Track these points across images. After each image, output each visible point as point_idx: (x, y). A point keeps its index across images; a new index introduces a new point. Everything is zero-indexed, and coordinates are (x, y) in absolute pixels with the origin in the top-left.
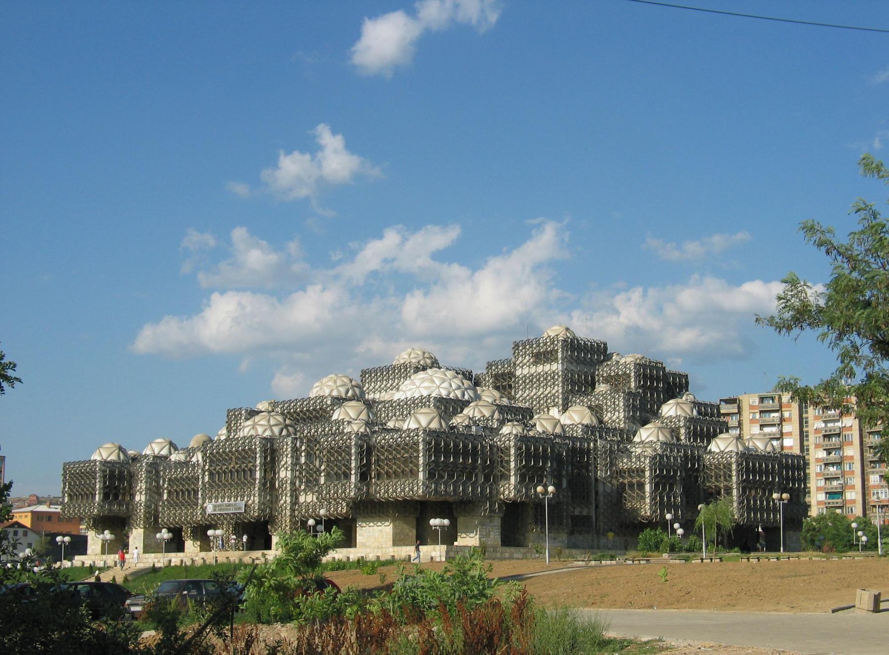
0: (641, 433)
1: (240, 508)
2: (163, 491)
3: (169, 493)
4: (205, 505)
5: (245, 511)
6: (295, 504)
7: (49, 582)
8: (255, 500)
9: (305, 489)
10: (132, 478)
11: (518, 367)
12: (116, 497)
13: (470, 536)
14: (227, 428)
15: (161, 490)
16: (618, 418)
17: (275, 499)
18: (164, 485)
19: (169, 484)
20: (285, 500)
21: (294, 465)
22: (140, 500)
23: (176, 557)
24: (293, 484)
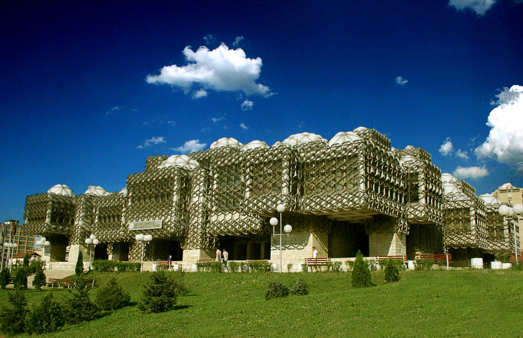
0: (449, 177)
1: (158, 225)
2: (95, 218)
3: (100, 218)
4: (128, 224)
5: (162, 228)
6: (206, 223)
7: (153, 138)
8: (172, 218)
9: (216, 211)
10: (73, 207)
11: (195, 195)
12: (61, 221)
13: (299, 248)
14: (127, 188)
15: (94, 216)
16: (196, 222)
17: (187, 221)
18: (96, 212)
19: (100, 212)
20: (197, 220)
21: (206, 192)
22: (78, 224)
23: (176, 264)
24: (204, 206)
